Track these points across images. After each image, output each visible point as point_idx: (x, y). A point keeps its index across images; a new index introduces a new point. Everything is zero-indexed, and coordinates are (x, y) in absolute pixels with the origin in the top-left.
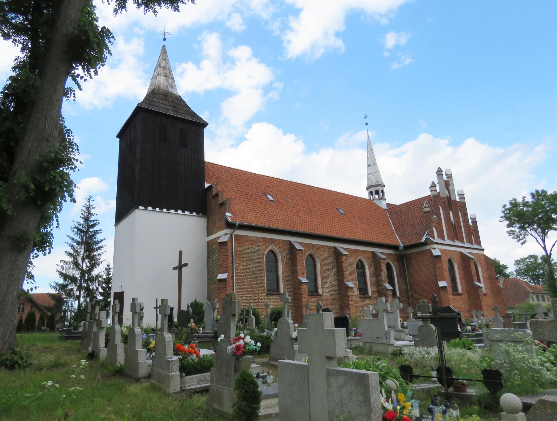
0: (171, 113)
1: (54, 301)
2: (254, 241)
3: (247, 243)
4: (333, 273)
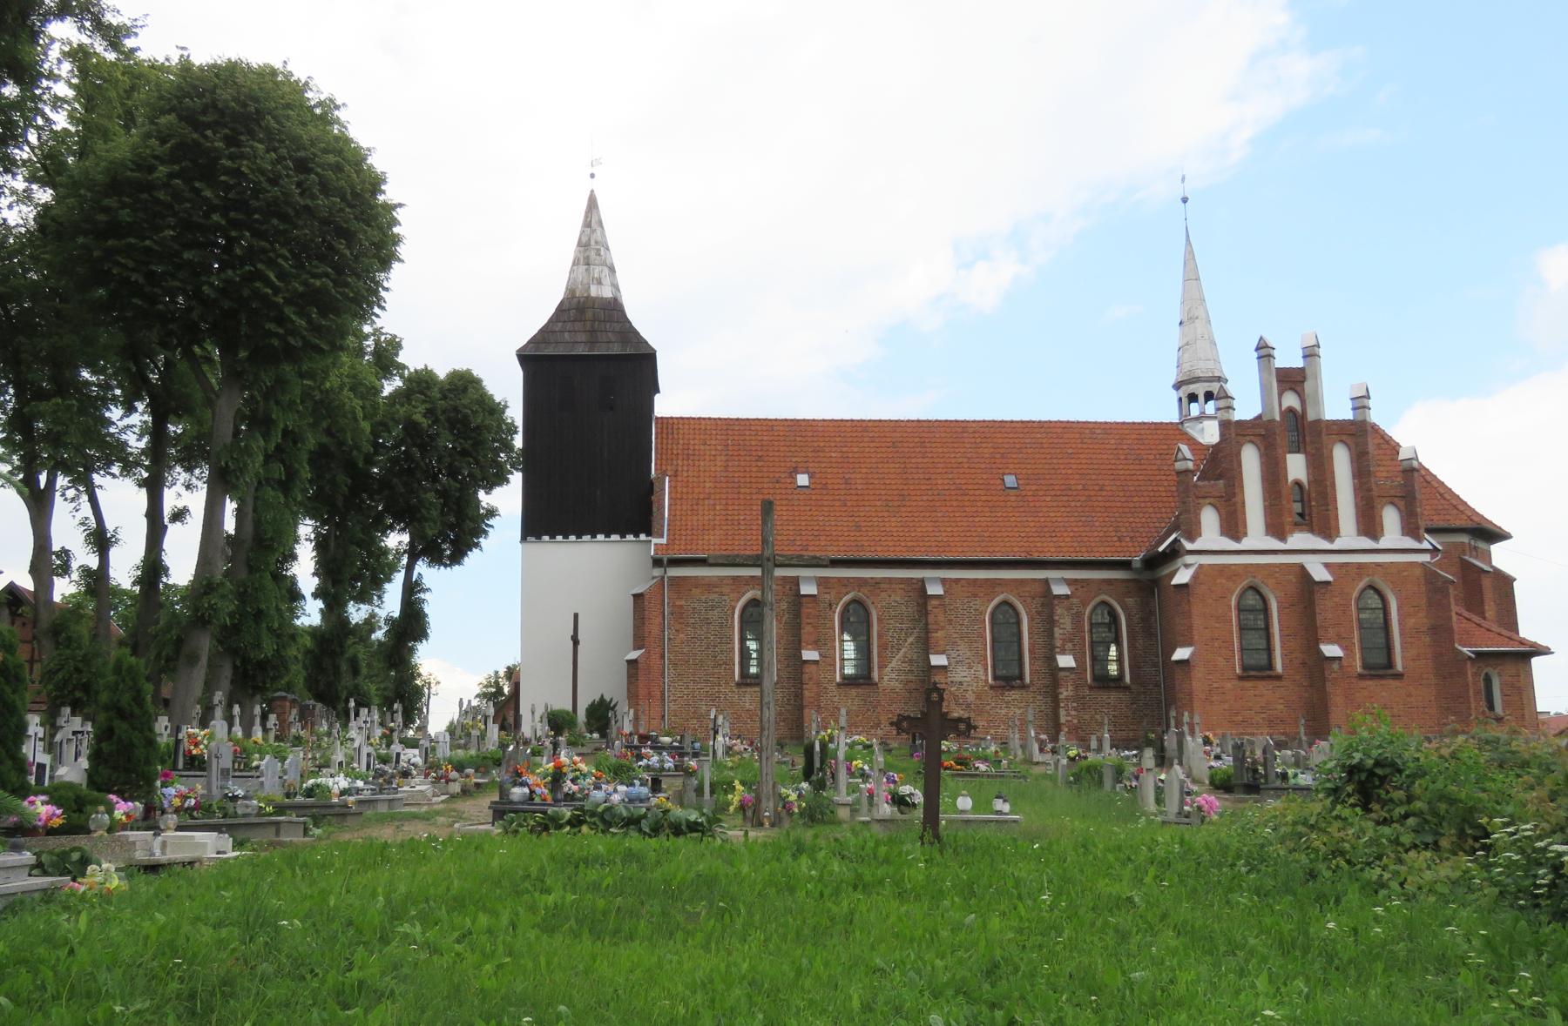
0: (581, 350)
1: (294, 577)
2: (709, 585)
3: (695, 591)
4: (915, 635)
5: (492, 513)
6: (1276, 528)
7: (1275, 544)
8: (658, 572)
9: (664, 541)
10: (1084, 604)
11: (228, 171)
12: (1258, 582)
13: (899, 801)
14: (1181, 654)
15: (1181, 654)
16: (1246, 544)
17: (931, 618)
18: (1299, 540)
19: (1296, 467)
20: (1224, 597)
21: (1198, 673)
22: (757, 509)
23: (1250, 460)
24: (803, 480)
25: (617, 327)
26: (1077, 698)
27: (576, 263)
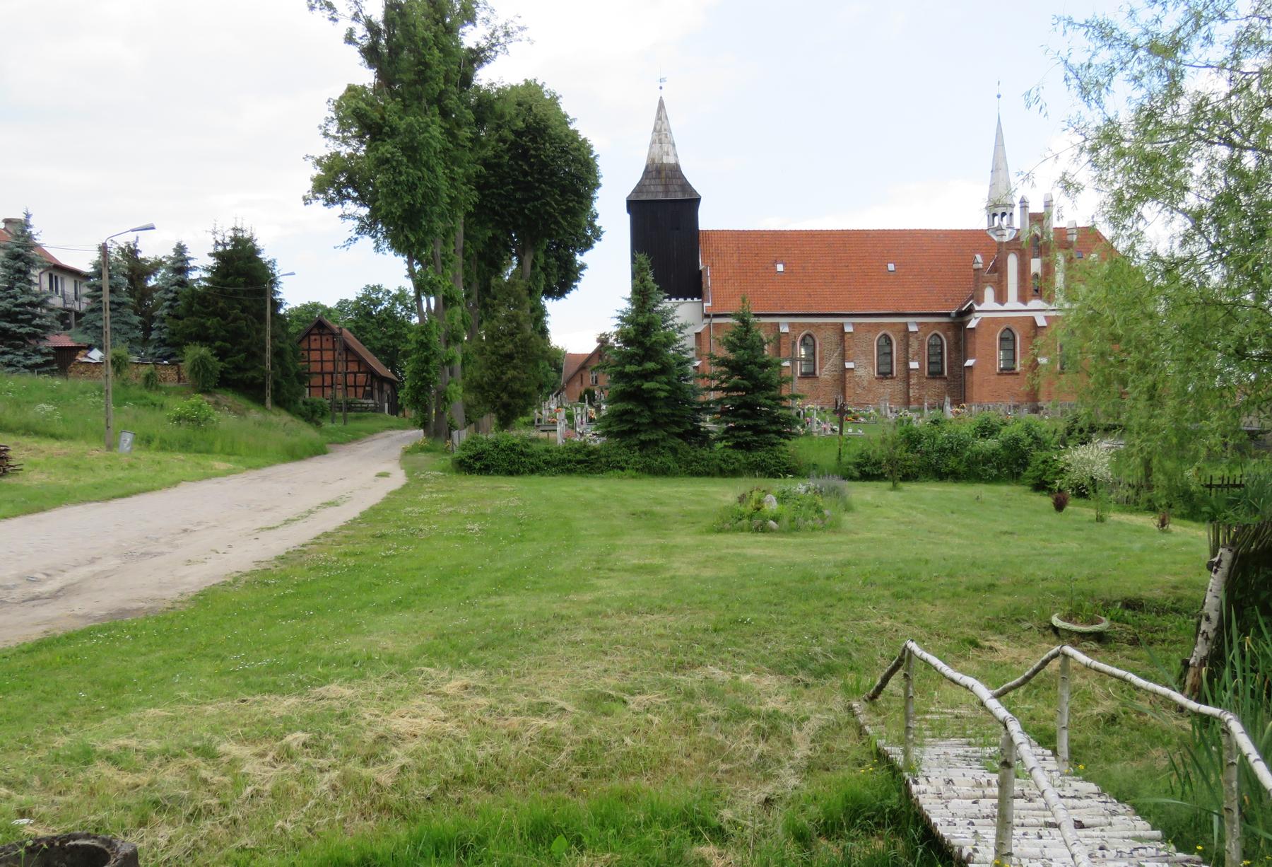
0: (661, 197)
5: (583, 267)
6: (1023, 298)
7: (1021, 306)
8: (707, 321)
9: (709, 304)
10: (926, 335)
11: (532, 156)
12: (1009, 326)
13: (833, 430)
14: (969, 363)
15: (969, 363)
16: (1007, 306)
17: (846, 344)
18: (1035, 304)
19: (1036, 265)
20: (993, 334)
21: (976, 372)
22: (1081, 832)
23: (1012, 262)
24: (780, 268)
25: (679, 182)
26: (919, 383)
27: (653, 142)
